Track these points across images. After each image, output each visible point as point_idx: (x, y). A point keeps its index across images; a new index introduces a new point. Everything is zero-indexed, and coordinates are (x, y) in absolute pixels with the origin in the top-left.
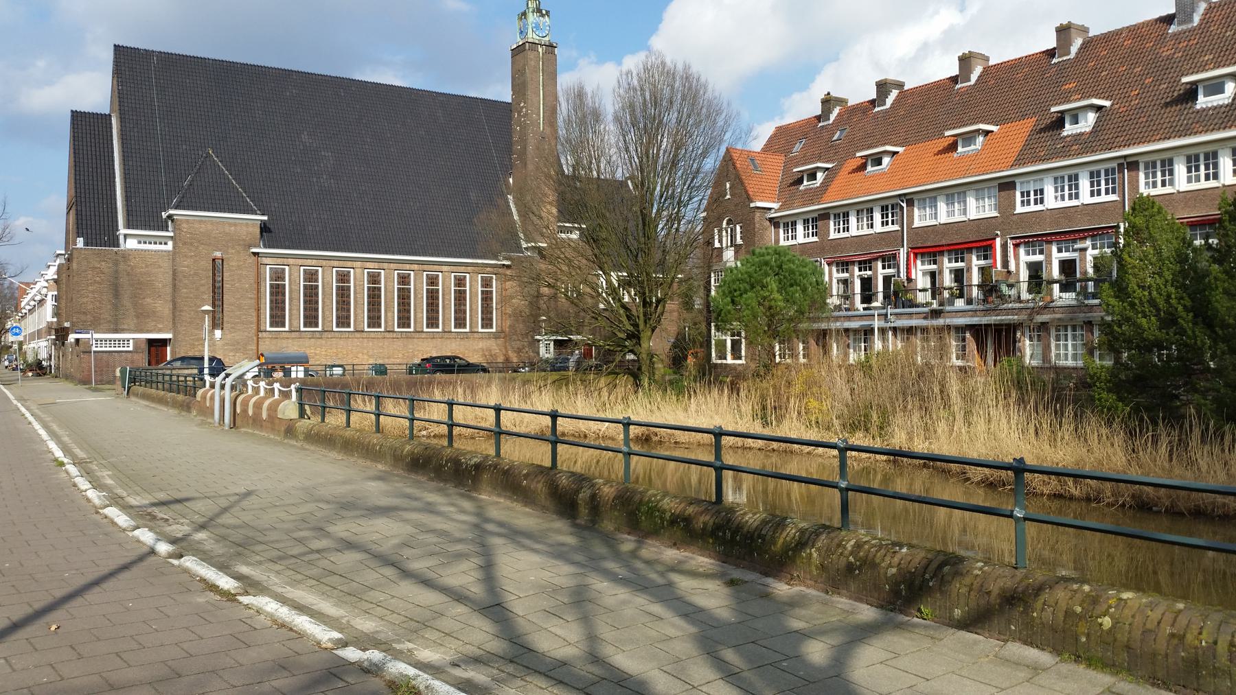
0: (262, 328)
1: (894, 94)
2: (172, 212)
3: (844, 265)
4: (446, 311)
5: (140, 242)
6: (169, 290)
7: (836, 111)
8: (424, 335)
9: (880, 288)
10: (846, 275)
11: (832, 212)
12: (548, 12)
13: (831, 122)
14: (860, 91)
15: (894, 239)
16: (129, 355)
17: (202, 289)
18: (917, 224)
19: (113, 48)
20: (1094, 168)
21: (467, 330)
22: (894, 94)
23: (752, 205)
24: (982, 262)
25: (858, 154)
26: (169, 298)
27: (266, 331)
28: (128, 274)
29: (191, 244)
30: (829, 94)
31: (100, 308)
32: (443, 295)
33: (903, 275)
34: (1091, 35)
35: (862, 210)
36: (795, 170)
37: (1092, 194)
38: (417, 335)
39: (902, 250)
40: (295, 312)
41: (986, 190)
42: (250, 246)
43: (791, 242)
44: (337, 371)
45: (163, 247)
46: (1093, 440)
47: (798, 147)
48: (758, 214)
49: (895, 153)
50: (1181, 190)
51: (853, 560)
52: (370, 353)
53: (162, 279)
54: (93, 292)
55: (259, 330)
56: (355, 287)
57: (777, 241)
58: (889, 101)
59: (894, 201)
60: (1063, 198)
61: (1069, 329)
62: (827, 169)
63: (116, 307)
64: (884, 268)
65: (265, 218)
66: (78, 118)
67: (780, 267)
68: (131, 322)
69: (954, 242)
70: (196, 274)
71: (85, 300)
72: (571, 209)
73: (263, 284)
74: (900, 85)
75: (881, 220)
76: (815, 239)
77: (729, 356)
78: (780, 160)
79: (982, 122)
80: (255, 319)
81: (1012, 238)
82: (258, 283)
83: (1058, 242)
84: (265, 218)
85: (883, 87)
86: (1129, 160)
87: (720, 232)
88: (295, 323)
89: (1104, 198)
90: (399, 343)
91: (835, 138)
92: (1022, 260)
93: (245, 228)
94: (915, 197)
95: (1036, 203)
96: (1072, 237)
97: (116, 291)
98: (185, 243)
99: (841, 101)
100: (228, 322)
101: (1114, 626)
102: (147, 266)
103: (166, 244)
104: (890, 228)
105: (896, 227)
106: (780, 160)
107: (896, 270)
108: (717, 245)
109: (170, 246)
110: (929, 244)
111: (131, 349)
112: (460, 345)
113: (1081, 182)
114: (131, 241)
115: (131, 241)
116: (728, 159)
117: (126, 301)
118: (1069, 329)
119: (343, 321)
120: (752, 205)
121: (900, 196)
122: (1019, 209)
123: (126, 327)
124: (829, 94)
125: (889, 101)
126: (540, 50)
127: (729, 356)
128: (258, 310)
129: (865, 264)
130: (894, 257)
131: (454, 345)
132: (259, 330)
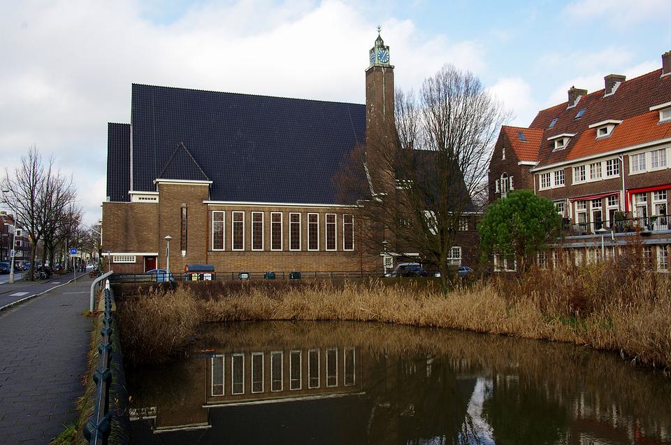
0: (210, 249)
1: (618, 84)
2: (157, 180)
3: (583, 201)
4: (322, 238)
5: (140, 199)
6: (156, 226)
7: (579, 98)
8: (326, 254)
9: (608, 218)
10: (584, 210)
12: (388, 47)
13: (575, 106)
14: (594, 84)
15: (615, 184)
16: (134, 265)
17: (175, 226)
18: (631, 173)
19: (131, 85)
21: (282, 250)
22: (618, 84)
23: (519, 163)
24: (659, 201)
26: (156, 231)
27: (211, 251)
28: (133, 217)
29: (169, 199)
30: (573, 87)
31: (118, 238)
32: (320, 227)
33: (623, 209)
34: (626, 80)
35: (594, 165)
36: (548, 139)
38: (304, 253)
39: (621, 192)
40: (228, 239)
42: (202, 200)
43: (546, 188)
44: (245, 276)
45: (153, 201)
47: (553, 123)
48: (523, 170)
49: (616, 124)
50: (605, 179)
52: (274, 265)
53: (153, 221)
54: (114, 228)
55: (208, 251)
56: (265, 223)
57: (538, 187)
58: (614, 90)
59: (615, 157)
62: (571, 137)
63: (126, 237)
65: (212, 182)
66: (113, 128)
67: (525, 205)
68: (135, 246)
70: (172, 217)
71: (109, 233)
72: (399, 173)
73: (210, 222)
74: (622, 78)
75: (586, 175)
76: (563, 185)
78: (540, 132)
79: (610, 119)
80: (205, 244)
82: (208, 222)
84: (212, 182)
85: (610, 80)
87: (499, 182)
88: (229, 247)
90: (292, 258)
91: (578, 116)
92: (637, 204)
93: (199, 189)
94: (629, 154)
97: (126, 227)
98: (166, 199)
99: (583, 92)
100: (190, 246)
102: (144, 212)
103: (155, 199)
104: (613, 176)
105: (618, 176)
106: (540, 132)
107: (618, 206)
108: (497, 190)
109: (157, 201)
110: (640, 186)
111: (135, 262)
112: (331, 260)
114: (136, 197)
115: (136, 197)
116: (505, 132)
117: (132, 233)
119: (258, 244)
120: (519, 163)
121: (619, 153)
123: (132, 249)
124: (573, 87)
125: (614, 90)
126: (383, 71)
128: (208, 238)
129: (598, 201)
130: (617, 196)
131: (327, 260)
132: (208, 251)
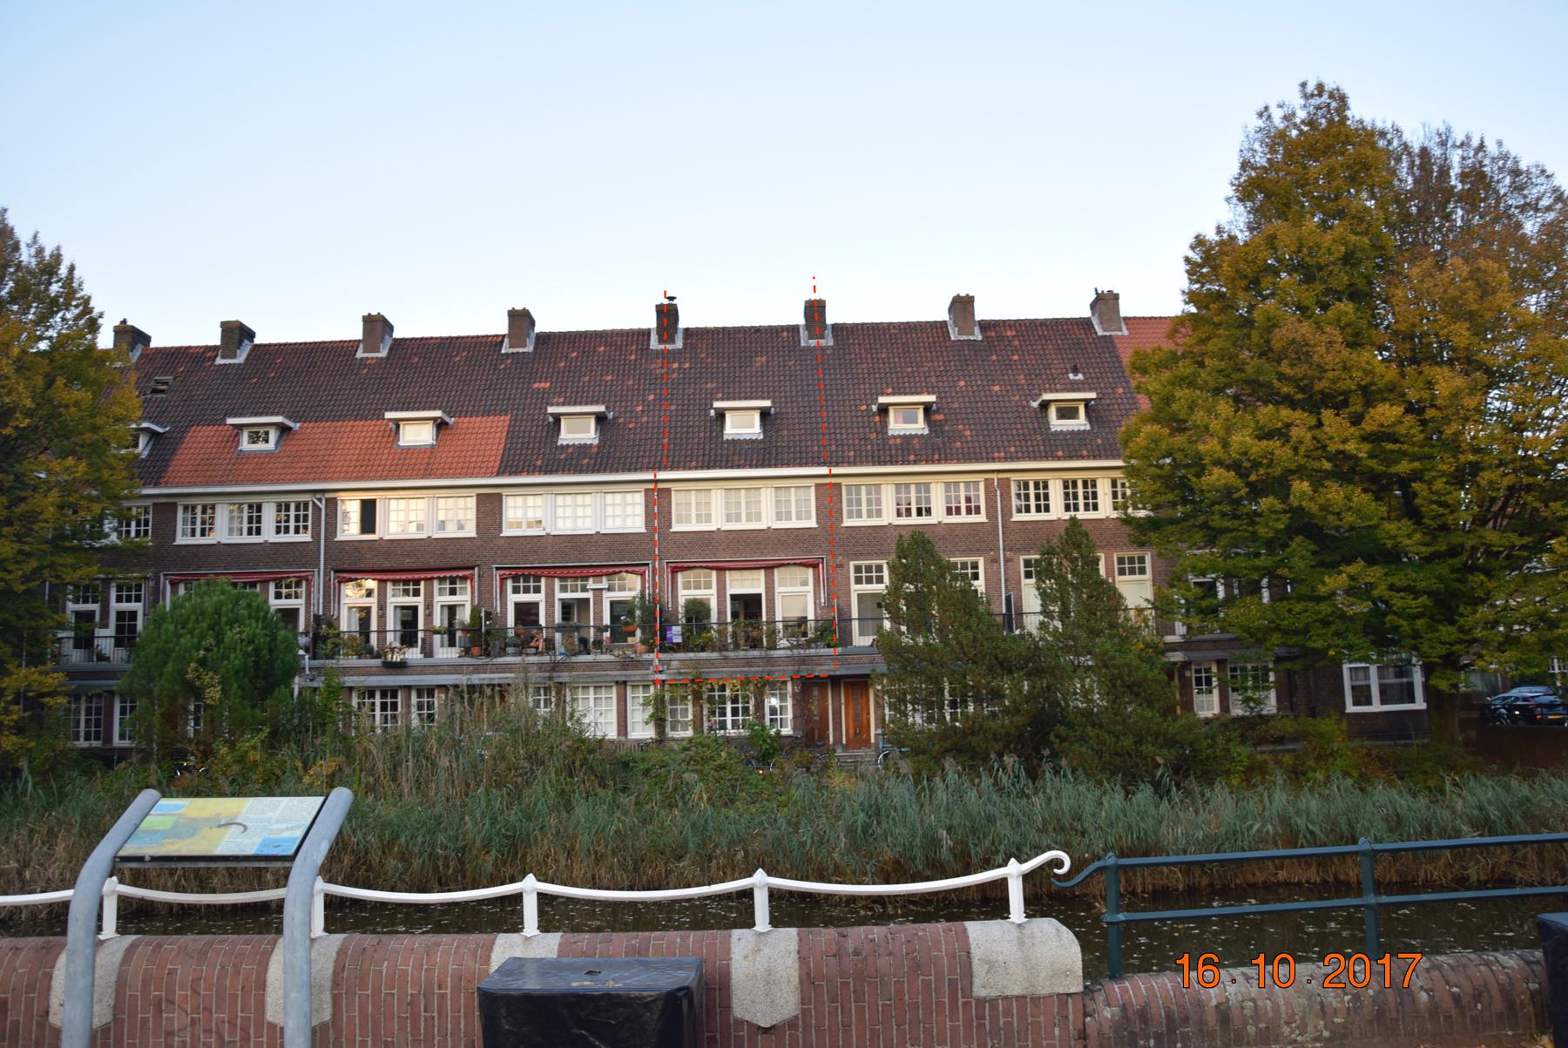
11: (181, 502)
20: (1070, 476)
25: (230, 421)
37: (278, 531)
41: (793, 490)
46: (1514, 783)
51: (1537, 986)
60: (193, 533)
61: (83, 699)
64: (119, 599)
69: (406, 566)
77: (82, 739)
81: (497, 569)
83: (562, 578)
86: (660, 486)
89: (291, 537)
95: (250, 533)
96: (611, 570)
101: (1431, 998)
105: (305, 537)
113: (1051, 491)
118: (83, 699)
122: (181, 540)
124: (124, 322)
127: (82, 739)
